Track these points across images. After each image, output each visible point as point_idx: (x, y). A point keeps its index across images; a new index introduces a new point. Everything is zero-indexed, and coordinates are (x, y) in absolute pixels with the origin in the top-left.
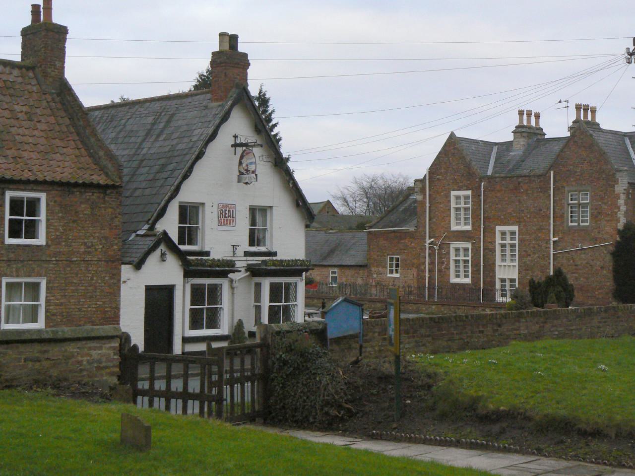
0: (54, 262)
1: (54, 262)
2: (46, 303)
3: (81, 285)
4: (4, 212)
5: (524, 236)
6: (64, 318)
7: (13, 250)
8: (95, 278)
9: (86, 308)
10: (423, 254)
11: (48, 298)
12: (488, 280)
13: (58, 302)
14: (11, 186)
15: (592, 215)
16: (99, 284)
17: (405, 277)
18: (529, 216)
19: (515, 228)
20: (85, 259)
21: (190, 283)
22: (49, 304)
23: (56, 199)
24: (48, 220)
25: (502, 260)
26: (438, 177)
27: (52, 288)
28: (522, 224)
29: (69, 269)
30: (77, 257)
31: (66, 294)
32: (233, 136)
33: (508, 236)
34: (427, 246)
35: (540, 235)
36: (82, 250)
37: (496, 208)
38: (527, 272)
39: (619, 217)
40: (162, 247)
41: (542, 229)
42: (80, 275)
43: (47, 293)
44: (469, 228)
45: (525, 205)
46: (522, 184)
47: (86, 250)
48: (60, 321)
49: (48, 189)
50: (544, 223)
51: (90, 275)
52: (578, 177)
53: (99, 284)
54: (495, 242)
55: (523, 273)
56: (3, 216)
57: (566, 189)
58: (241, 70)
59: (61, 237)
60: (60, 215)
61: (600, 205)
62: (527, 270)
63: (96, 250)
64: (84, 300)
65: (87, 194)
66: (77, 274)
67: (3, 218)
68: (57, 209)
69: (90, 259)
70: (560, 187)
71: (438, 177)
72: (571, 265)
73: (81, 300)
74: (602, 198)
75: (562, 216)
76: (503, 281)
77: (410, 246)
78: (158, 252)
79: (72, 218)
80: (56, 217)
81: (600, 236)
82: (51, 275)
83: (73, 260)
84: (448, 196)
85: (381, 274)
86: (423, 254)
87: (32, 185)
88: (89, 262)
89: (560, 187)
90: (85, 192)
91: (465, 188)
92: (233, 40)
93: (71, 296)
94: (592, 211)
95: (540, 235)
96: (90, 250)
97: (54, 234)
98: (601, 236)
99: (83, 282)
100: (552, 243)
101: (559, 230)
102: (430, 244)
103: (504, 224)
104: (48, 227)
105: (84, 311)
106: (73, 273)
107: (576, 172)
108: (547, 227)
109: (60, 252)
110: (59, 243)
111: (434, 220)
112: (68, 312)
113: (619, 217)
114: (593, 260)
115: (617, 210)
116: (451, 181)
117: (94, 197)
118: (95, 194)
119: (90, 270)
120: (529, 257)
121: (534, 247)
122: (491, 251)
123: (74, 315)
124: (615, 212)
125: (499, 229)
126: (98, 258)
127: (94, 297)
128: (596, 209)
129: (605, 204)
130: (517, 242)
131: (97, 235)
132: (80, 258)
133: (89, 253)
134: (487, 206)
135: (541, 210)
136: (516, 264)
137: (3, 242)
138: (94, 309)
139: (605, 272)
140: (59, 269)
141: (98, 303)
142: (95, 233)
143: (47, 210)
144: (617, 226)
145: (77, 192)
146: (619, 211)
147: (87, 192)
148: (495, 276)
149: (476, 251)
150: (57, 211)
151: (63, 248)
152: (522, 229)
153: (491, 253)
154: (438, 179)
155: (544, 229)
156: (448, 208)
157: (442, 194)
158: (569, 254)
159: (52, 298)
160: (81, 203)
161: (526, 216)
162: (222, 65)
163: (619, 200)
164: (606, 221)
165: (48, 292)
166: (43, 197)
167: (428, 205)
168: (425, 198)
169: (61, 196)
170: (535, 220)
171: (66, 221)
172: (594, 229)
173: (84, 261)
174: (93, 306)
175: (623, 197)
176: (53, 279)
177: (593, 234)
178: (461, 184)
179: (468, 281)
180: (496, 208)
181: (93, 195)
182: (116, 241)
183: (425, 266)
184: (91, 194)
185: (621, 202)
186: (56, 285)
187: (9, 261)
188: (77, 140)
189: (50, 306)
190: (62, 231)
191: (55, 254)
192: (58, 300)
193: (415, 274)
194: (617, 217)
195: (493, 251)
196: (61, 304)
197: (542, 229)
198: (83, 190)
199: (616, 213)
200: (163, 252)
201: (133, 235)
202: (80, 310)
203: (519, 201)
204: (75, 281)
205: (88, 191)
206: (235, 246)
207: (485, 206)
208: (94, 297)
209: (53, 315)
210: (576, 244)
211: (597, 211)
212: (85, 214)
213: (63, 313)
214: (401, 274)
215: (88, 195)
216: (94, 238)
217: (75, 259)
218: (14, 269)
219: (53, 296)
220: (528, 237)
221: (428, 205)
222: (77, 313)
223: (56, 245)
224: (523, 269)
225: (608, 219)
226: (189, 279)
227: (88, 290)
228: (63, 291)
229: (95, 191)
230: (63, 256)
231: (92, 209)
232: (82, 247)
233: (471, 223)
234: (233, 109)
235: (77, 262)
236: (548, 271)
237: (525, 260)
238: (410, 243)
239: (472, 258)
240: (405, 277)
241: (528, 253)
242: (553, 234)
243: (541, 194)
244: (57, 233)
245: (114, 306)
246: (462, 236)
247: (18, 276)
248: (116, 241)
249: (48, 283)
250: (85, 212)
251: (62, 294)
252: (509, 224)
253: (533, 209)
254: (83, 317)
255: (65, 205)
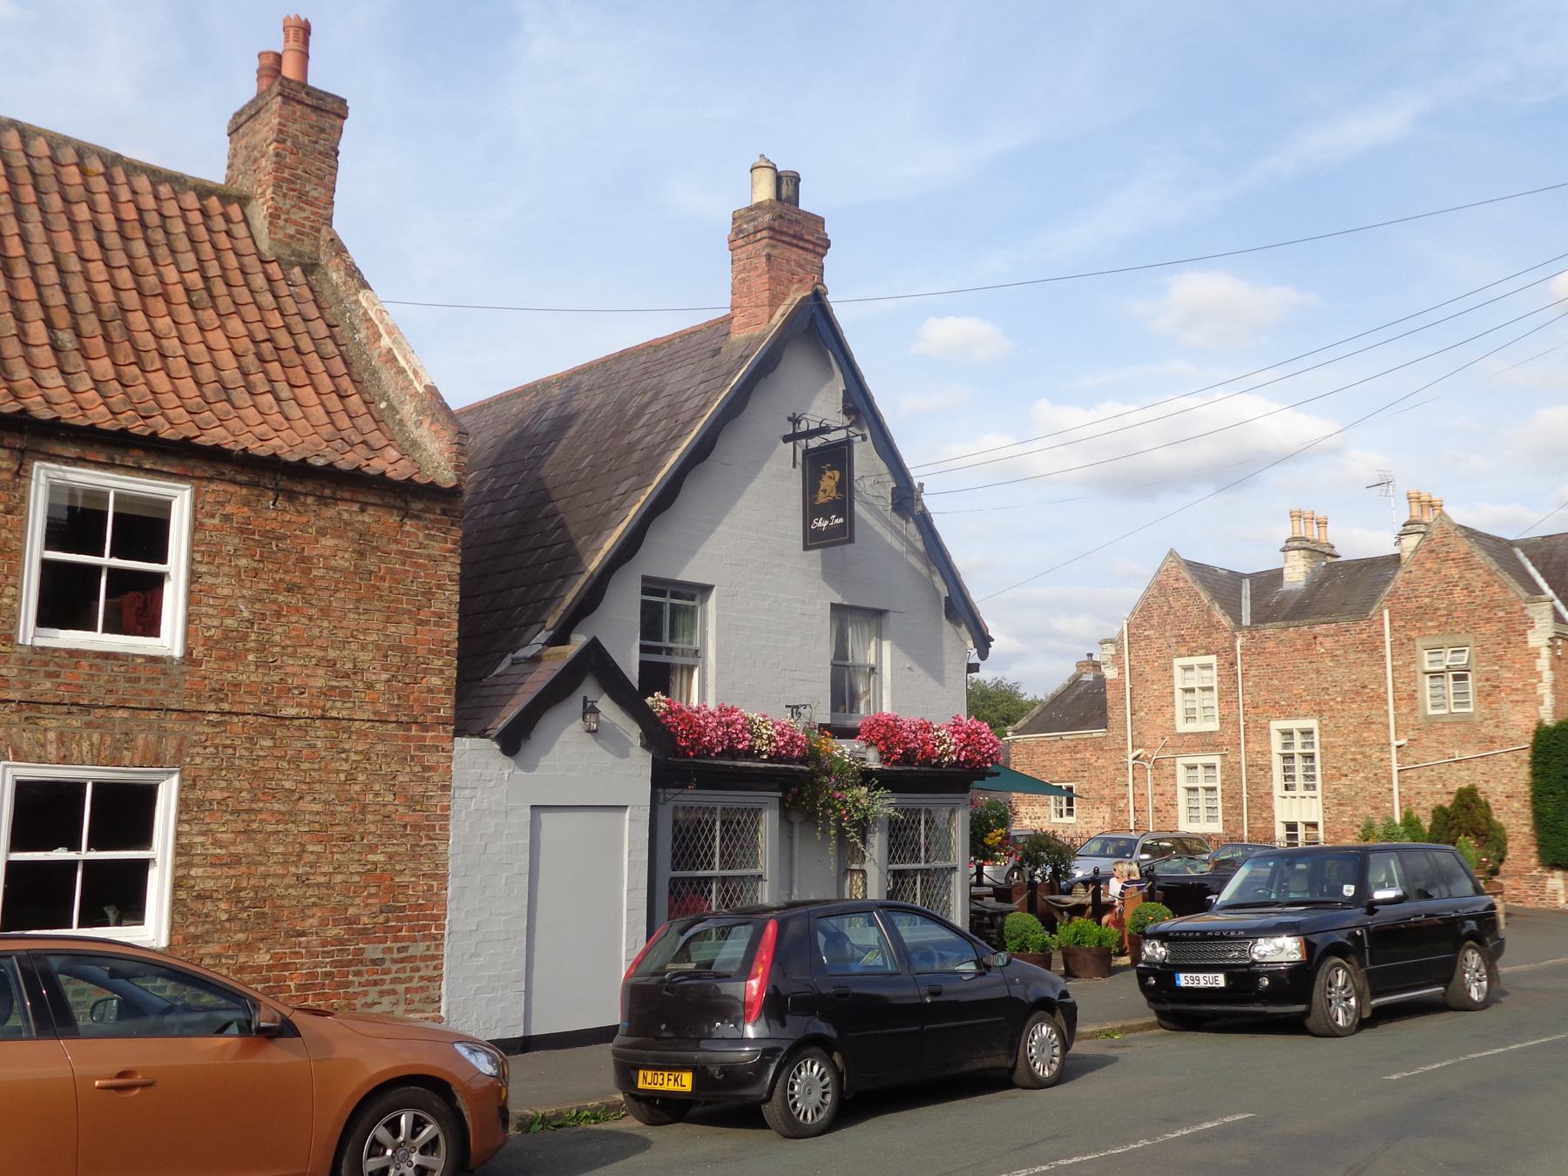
0: (211, 717)
1: (211, 717)
2: (177, 854)
3: (309, 798)
4: (21, 530)
5: (1331, 739)
6: (245, 909)
7: (52, 668)
8: (361, 777)
9: (325, 874)
10: (1122, 779)
11: (184, 840)
12: (1259, 826)
13: (223, 852)
14: (58, 449)
15: (1479, 692)
16: (377, 795)
17: (1086, 823)
18: (1339, 699)
19: (1312, 723)
20: (328, 715)
21: (670, 805)
22: (184, 859)
23: (229, 509)
24: (193, 577)
25: (1287, 788)
26: (1146, 633)
27: (200, 804)
28: (1326, 715)
29: (268, 743)
30: (299, 705)
31: (255, 826)
32: (789, 419)
33: (1298, 739)
34: (1131, 762)
35: (1365, 735)
36: (319, 683)
37: (1268, 685)
38: (1342, 808)
39: (1542, 696)
40: (588, 689)
41: (1370, 723)
42: (305, 766)
43: (179, 821)
44: (1214, 726)
45: (1330, 679)
46: (1320, 639)
47: (334, 683)
48: (228, 920)
49: (198, 473)
50: (1374, 712)
51: (346, 766)
52: (1444, 619)
53: (377, 795)
54: (1270, 752)
55: (1334, 810)
56: (14, 545)
57: (1419, 643)
58: (809, 256)
59: (244, 638)
60: (243, 562)
61: (1497, 671)
62: (1342, 805)
63: (370, 686)
64: (319, 848)
65: (342, 507)
66: (295, 761)
67: (12, 554)
68: (232, 542)
69: (344, 714)
70: (1405, 641)
71: (1146, 633)
72: (1438, 793)
73: (310, 848)
74: (1500, 658)
75: (1412, 696)
76: (1291, 827)
77: (1095, 764)
78: (575, 704)
79: (287, 578)
80: (226, 569)
81: (1501, 732)
82: (198, 760)
83: (284, 713)
84: (1167, 668)
85: (1039, 818)
86: (1122, 779)
87: (138, 453)
88: (344, 723)
89: (1405, 641)
90: (336, 500)
91: (1203, 651)
92: (786, 184)
93: (270, 834)
94: (1480, 684)
95: (1365, 735)
96: (345, 683)
97: (216, 623)
98: (1501, 734)
99: (317, 787)
100: (1394, 750)
101: (1408, 724)
102: (1134, 759)
103: (1288, 716)
104: (192, 598)
105: (319, 885)
106: (282, 758)
107: (1438, 609)
108: (1382, 719)
109: (237, 685)
110: (237, 656)
111: (1142, 714)
112: (256, 889)
113: (1542, 696)
114: (1487, 782)
115: (1535, 681)
116: (1174, 640)
117: (366, 519)
118: (371, 510)
119: (344, 751)
120: (1343, 778)
121: (1354, 760)
122: (1262, 770)
123: (283, 897)
124: (1531, 684)
125: (1276, 725)
126: (375, 713)
127: (357, 838)
128: (1487, 680)
129: (1509, 669)
130: (1317, 751)
131: (374, 637)
132: (311, 707)
133: (345, 694)
134: (1250, 684)
135: (1364, 687)
136: (1318, 792)
137: (10, 638)
138: (356, 879)
139: (1516, 805)
140: (228, 742)
141: (371, 857)
142: (366, 631)
143: (194, 544)
144: (1538, 713)
145: (306, 495)
146: (1541, 681)
147: (343, 500)
148: (1273, 817)
149: (1231, 771)
150: (231, 548)
151: (248, 673)
152: (1326, 725)
153: (1262, 772)
154: (1147, 638)
155: (1373, 723)
156: (1168, 690)
157: (1157, 664)
158: (1432, 770)
159: (199, 839)
160: (322, 532)
161: (1333, 699)
162: (759, 236)
163: (1538, 660)
164: (1511, 701)
165: (184, 817)
166: (181, 502)
167: (1128, 685)
168: (1121, 673)
169: (246, 503)
170: (1354, 706)
171: (262, 586)
172: (1486, 719)
173: (323, 718)
174: (353, 868)
175: (1545, 652)
176: (205, 774)
177: (1483, 731)
178: (1194, 644)
179: (1216, 828)
180: (1268, 685)
181: (363, 510)
182: (438, 663)
183: (1125, 801)
184: (355, 507)
185: (1543, 663)
186: (218, 795)
187: (33, 704)
188: (220, 232)
189: (189, 865)
190: (246, 614)
191: (218, 693)
192: (221, 847)
193: (1107, 818)
194: (1535, 693)
195: (1267, 768)
196: (236, 860)
197: (1370, 723)
198: (328, 492)
199: (1534, 686)
200: (589, 705)
201: (507, 661)
202: (302, 880)
203: (1318, 671)
204: (287, 785)
205: (347, 495)
206: (797, 707)
207: (1245, 684)
208: (357, 838)
209: (201, 897)
210: (1447, 751)
211: (1489, 683)
212: (335, 569)
213: (238, 889)
214: (1078, 818)
215: (346, 511)
216: (363, 647)
217: (292, 712)
218: (51, 736)
219: (203, 834)
220: (1341, 739)
221: (1128, 685)
222: (292, 892)
223: (223, 659)
224: (1336, 802)
225: (1516, 698)
226: (667, 791)
227: (333, 814)
228: (245, 817)
229: (372, 500)
230: (248, 699)
231: (361, 554)
232: (320, 672)
233: (1217, 717)
234: (784, 355)
235: (296, 722)
236: (1387, 805)
237: (1335, 784)
238: (1095, 758)
239: (1223, 784)
240: (1086, 823)
241: (1343, 772)
242: (1396, 731)
243: (1364, 656)
244: (229, 622)
245: (425, 869)
246: (1204, 742)
247: (64, 760)
248: (438, 663)
249: (186, 787)
250: (333, 563)
251: (241, 826)
252: (1297, 717)
253: (1348, 684)
254: (314, 904)
255: (264, 534)
